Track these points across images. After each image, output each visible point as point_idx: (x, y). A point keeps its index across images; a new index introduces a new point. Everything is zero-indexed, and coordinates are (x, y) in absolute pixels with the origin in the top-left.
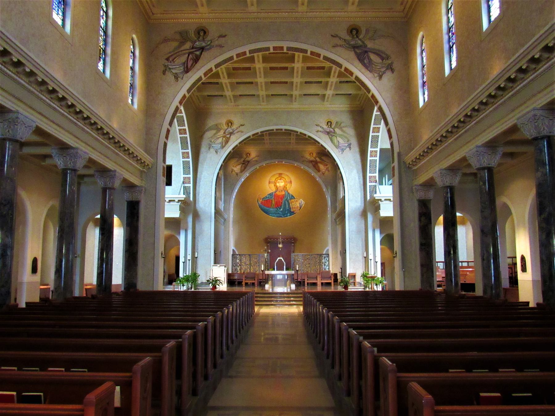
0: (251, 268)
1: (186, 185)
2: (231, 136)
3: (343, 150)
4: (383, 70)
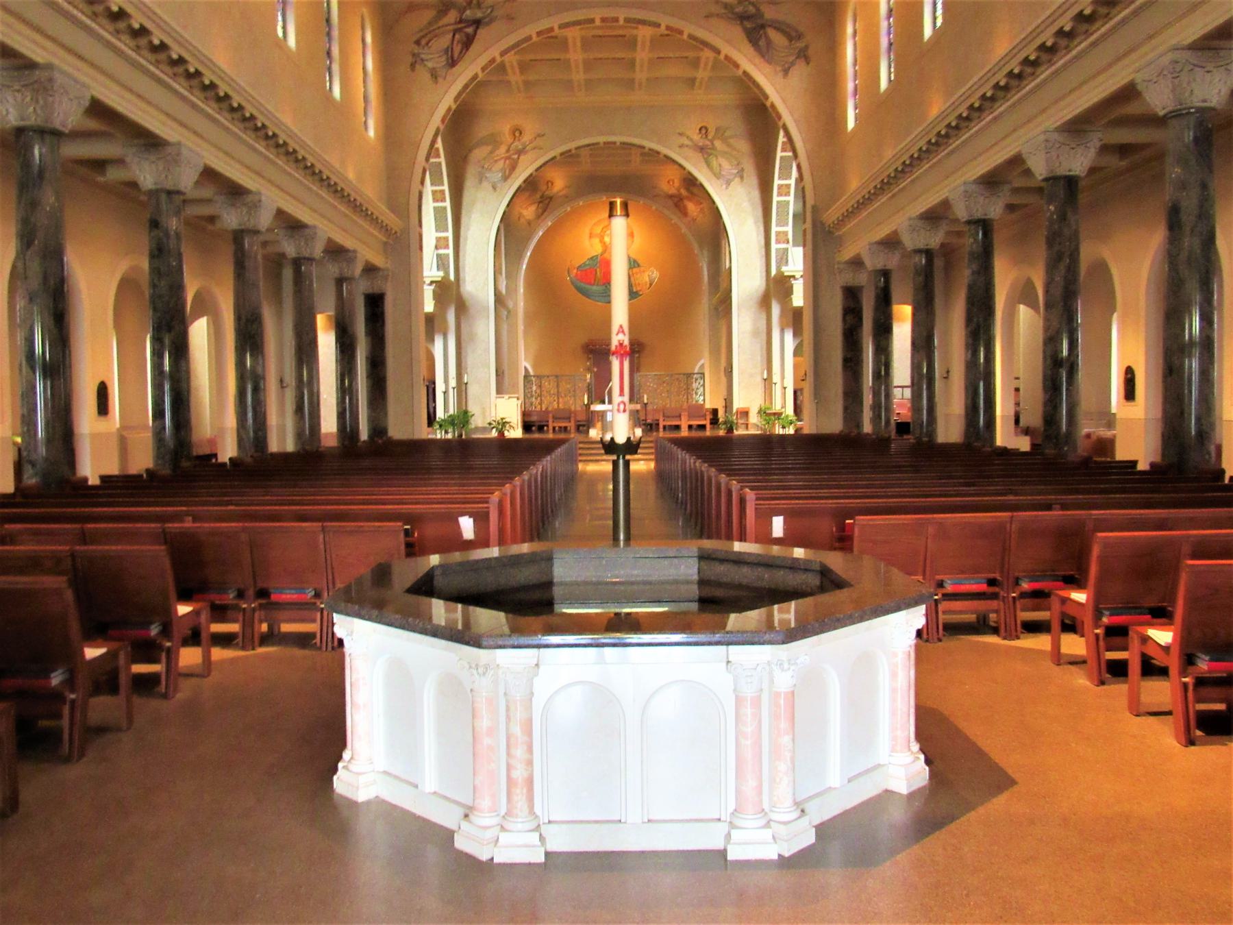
0: (561, 400)
1: (442, 251)
2: (479, 32)
3: (728, 183)
4: (791, 59)
